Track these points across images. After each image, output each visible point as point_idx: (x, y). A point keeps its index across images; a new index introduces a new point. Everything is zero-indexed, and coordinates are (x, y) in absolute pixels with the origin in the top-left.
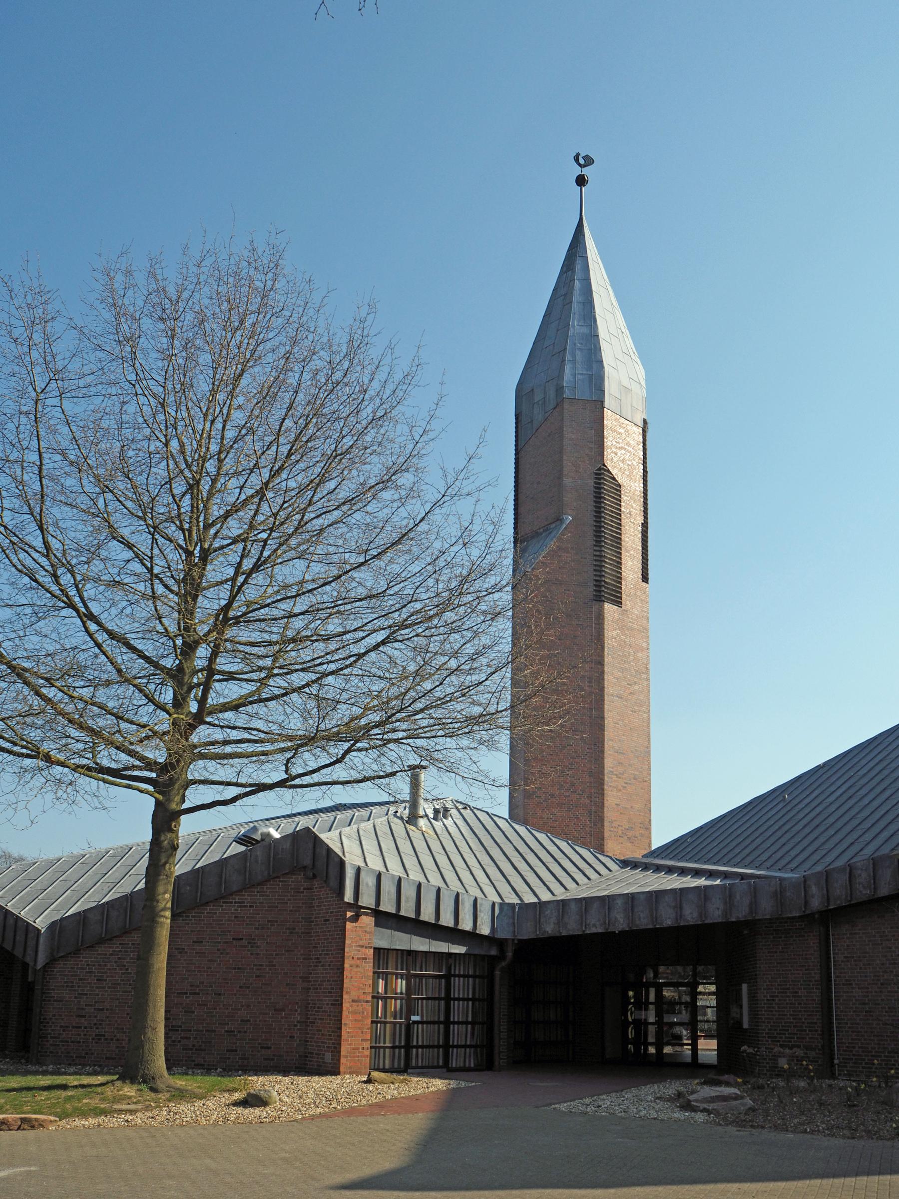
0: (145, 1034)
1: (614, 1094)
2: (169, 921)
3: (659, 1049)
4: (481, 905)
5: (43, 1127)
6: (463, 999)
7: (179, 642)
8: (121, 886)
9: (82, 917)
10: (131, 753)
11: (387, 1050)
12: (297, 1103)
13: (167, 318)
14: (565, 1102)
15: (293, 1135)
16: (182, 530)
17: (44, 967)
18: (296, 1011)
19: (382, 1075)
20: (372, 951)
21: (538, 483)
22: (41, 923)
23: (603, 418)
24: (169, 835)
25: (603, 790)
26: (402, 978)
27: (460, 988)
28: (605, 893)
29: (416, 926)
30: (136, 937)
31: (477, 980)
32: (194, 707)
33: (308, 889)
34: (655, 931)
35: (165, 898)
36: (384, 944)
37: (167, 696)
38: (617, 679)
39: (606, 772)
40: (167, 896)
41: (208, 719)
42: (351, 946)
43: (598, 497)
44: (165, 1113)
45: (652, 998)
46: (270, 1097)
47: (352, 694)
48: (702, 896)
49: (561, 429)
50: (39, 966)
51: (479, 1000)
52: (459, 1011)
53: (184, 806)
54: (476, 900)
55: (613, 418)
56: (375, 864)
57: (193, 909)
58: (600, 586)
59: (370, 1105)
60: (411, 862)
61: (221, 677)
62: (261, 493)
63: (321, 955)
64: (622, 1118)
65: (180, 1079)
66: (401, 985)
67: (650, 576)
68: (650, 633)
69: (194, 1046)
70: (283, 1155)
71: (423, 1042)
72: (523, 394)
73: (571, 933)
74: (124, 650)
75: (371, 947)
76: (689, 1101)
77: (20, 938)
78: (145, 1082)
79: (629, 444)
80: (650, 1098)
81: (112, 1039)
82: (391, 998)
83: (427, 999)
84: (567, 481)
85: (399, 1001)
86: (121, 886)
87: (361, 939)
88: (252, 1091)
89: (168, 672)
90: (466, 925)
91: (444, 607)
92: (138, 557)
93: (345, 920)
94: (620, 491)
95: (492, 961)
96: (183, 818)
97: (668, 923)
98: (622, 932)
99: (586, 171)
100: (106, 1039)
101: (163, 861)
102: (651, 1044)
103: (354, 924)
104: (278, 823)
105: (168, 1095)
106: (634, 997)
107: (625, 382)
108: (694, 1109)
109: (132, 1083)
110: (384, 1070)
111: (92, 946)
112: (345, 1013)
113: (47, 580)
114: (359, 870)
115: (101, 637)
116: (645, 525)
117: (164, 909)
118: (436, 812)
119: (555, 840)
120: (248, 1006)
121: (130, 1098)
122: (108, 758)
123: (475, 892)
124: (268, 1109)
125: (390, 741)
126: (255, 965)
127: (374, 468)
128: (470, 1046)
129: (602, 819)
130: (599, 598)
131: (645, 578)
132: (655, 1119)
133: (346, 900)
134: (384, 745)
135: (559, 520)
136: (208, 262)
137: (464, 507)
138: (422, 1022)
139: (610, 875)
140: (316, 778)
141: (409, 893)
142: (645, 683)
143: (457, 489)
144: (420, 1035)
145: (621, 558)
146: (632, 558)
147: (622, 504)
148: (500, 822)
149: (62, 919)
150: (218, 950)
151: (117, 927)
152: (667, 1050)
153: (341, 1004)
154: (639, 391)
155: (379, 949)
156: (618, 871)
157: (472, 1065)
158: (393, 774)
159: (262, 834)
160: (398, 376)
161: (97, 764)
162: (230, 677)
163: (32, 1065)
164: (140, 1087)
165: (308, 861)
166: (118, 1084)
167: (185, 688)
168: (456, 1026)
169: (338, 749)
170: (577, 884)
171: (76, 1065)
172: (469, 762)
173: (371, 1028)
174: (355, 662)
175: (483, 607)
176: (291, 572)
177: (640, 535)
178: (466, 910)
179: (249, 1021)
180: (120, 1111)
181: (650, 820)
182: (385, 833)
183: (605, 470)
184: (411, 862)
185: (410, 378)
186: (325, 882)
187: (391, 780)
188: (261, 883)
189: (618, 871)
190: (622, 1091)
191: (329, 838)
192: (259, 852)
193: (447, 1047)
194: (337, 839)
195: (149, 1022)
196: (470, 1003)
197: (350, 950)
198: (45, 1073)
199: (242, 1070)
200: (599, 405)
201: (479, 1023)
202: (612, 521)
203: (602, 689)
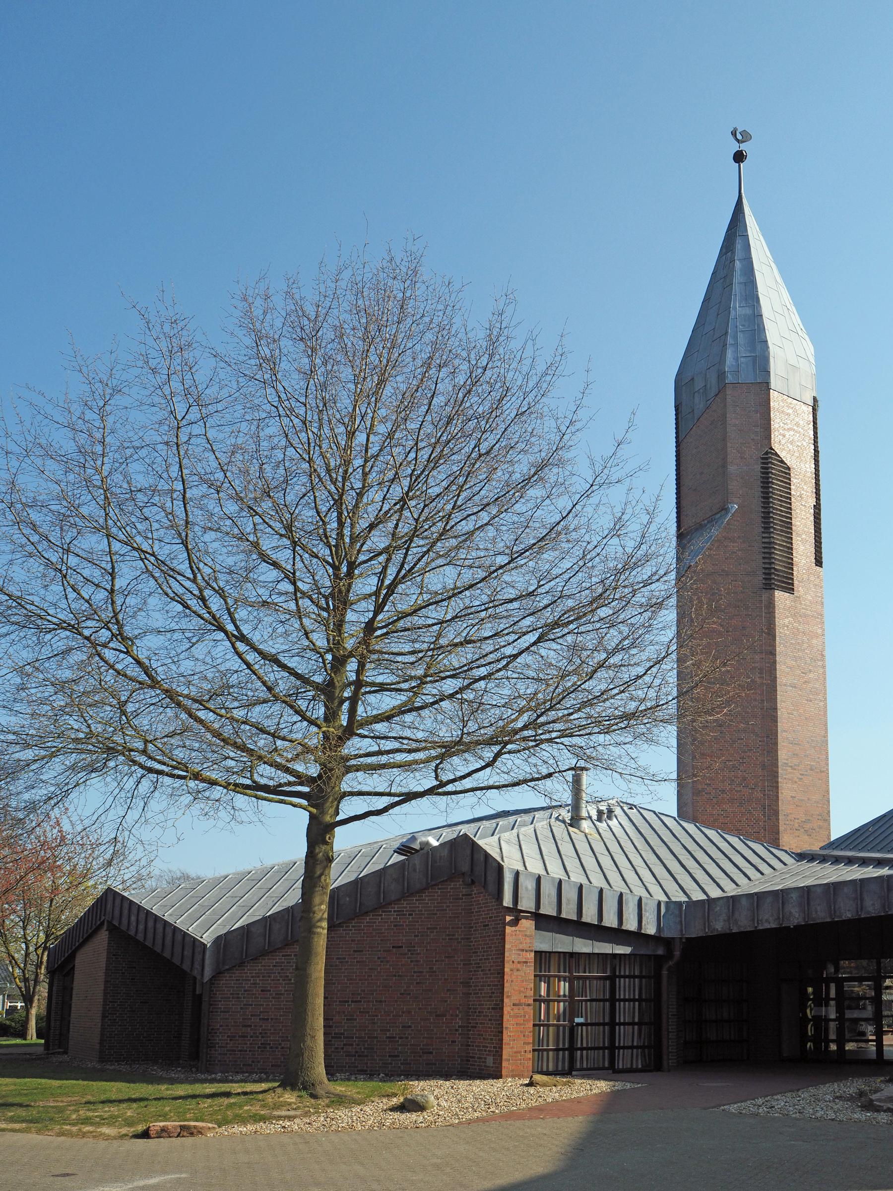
0: (304, 1041)
1: (789, 1094)
2: (326, 931)
3: (841, 1047)
4: (646, 904)
5: (202, 1134)
6: (629, 1000)
7: (329, 657)
8: (285, 900)
9: (246, 930)
10: (287, 770)
11: (551, 1053)
12: (455, 1108)
13: (309, 341)
14: (735, 1103)
15: (447, 1140)
16: (330, 547)
17: (211, 979)
18: (457, 1016)
19: (545, 1078)
20: (533, 954)
21: (702, 473)
22: (207, 939)
23: (769, 399)
24: (324, 847)
25: (778, 782)
26: (564, 981)
27: (624, 988)
28: (780, 887)
29: (578, 927)
30: (297, 948)
31: (644, 980)
32: (344, 720)
33: (466, 895)
34: (833, 924)
35: (322, 909)
36: (545, 947)
37: (320, 711)
38: (791, 668)
39: (780, 764)
40: (323, 907)
41: (360, 731)
42: (510, 950)
43: (766, 483)
44: (322, 1119)
45: (833, 994)
46: (427, 1102)
47: (501, 696)
48: (885, 886)
49: (724, 416)
50: (206, 979)
51: (645, 1000)
52: (624, 1012)
53: (338, 818)
54: (640, 900)
55: (780, 399)
56: (534, 867)
57: (353, 919)
58: (770, 574)
59: (530, 1109)
60: (572, 864)
61: (373, 689)
62: (403, 501)
63: (481, 960)
64: (796, 1119)
65: (340, 1085)
66: (563, 988)
67: (823, 560)
68: (825, 620)
69: (356, 1052)
70: (435, 1160)
71: (587, 1043)
72: (682, 384)
73: (742, 929)
74: (276, 668)
75: (531, 951)
76: (872, 1100)
77: (188, 953)
78: (305, 1088)
79: (797, 425)
80: (828, 1097)
81: (277, 1048)
82: (554, 1001)
83: (591, 1000)
84: (732, 469)
85: (562, 1004)
86: (285, 900)
87: (521, 943)
88: (409, 1097)
89: (317, 687)
90: (631, 925)
91: (597, 601)
92: (288, 578)
93: (504, 924)
94: (790, 474)
95: (659, 961)
96: (338, 830)
97: (849, 915)
98: (798, 927)
99: (743, 147)
100: (271, 1048)
101: (318, 873)
102: (833, 1041)
103: (514, 928)
104: (440, 833)
105: (327, 1101)
106: (813, 993)
107: (793, 361)
108: (878, 1110)
109: (293, 1089)
110: (547, 1073)
111: (256, 959)
112: (506, 1017)
113: (193, 603)
114: (517, 874)
115: (251, 657)
116: (817, 507)
117: (321, 920)
118: (600, 813)
119: (681, 822)
120: (409, 1012)
121: (290, 1104)
122: (266, 774)
123: (640, 891)
124: (425, 1113)
125: (542, 741)
126: (415, 972)
127: (522, 467)
128: (637, 1047)
129: (776, 813)
130: (769, 586)
131: (819, 562)
132: (833, 1120)
133: (505, 904)
134: (537, 746)
135: (724, 509)
136: (346, 275)
137: (615, 496)
138: (586, 1024)
139: (785, 869)
140: (467, 783)
141: (569, 895)
142: (821, 670)
143: (605, 477)
144: (584, 1037)
145: (792, 544)
146: (804, 542)
147: (792, 487)
148: (667, 820)
149: (228, 933)
150: (379, 958)
151: (274, 940)
152: (850, 1046)
153: (502, 1009)
154: (808, 368)
155: (541, 952)
156: (793, 864)
157: (640, 1066)
158: (550, 775)
159: (420, 843)
160: (541, 368)
161: (254, 782)
162: (382, 688)
163: (202, 1073)
164: (300, 1094)
165: (465, 867)
166: (279, 1090)
167: (336, 702)
168: (622, 1027)
169: (488, 754)
170: (749, 879)
171: (243, 1072)
172: (626, 760)
173: (534, 1031)
174: (508, 664)
175: (639, 598)
176: (441, 579)
177: (812, 518)
178: (631, 909)
179: (410, 1027)
180: (279, 1118)
181: (829, 812)
182: (546, 837)
183: (772, 454)
184: (572, 864)
185: (554, 369)
186: (484, 887)
187: (548, 782)
188: (422, 891)
189: (793, 864)
190: (798, 1090)
191: (488, 844)
192: (417, 860)
193: (612, 1048)
194: (496, 845)
195: (308, 1030)
196: (637, 1003)
197: (511, 954)
198: (212, 1081)
199: (404, 1075)
200: (766, 386)
201: (646, 1024)
202: (781, 506)
203: (774, 679)
